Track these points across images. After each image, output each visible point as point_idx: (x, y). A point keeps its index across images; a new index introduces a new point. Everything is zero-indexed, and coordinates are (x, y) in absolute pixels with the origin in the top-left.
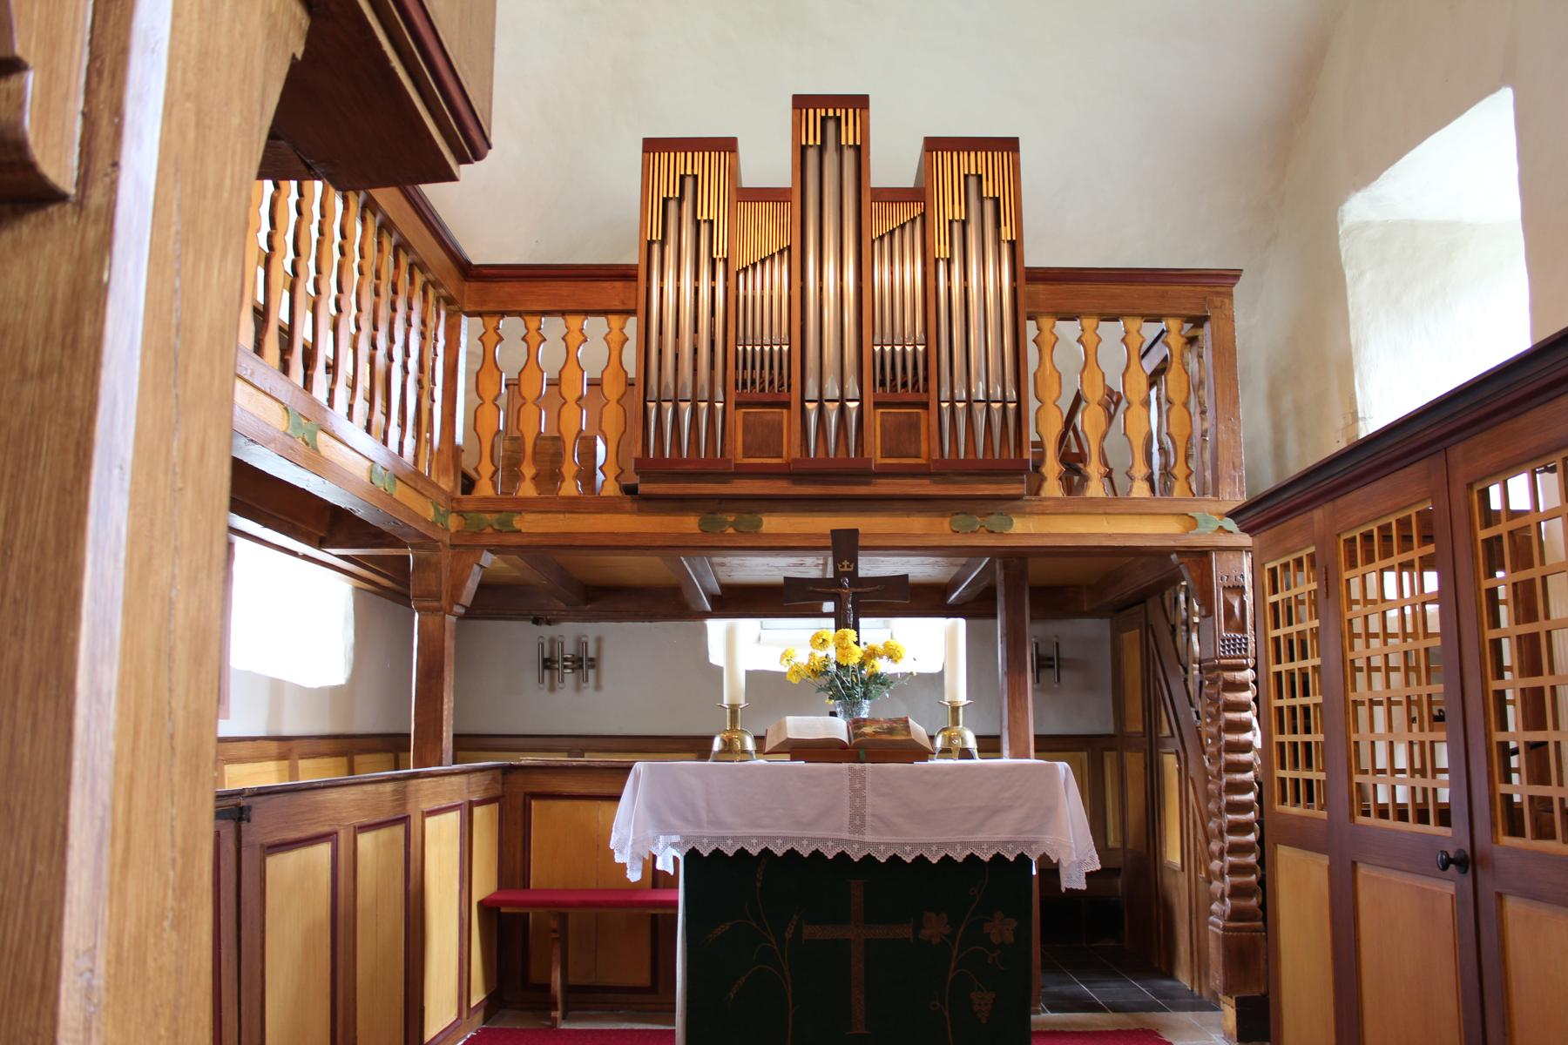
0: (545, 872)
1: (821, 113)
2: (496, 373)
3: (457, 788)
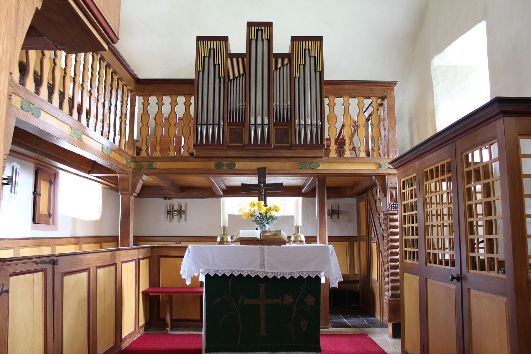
0: (165, 282)
1: (256, 28)
2: (148, 115)
3: (135, 254)
